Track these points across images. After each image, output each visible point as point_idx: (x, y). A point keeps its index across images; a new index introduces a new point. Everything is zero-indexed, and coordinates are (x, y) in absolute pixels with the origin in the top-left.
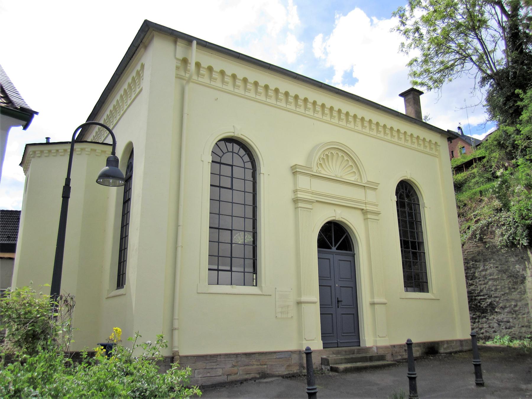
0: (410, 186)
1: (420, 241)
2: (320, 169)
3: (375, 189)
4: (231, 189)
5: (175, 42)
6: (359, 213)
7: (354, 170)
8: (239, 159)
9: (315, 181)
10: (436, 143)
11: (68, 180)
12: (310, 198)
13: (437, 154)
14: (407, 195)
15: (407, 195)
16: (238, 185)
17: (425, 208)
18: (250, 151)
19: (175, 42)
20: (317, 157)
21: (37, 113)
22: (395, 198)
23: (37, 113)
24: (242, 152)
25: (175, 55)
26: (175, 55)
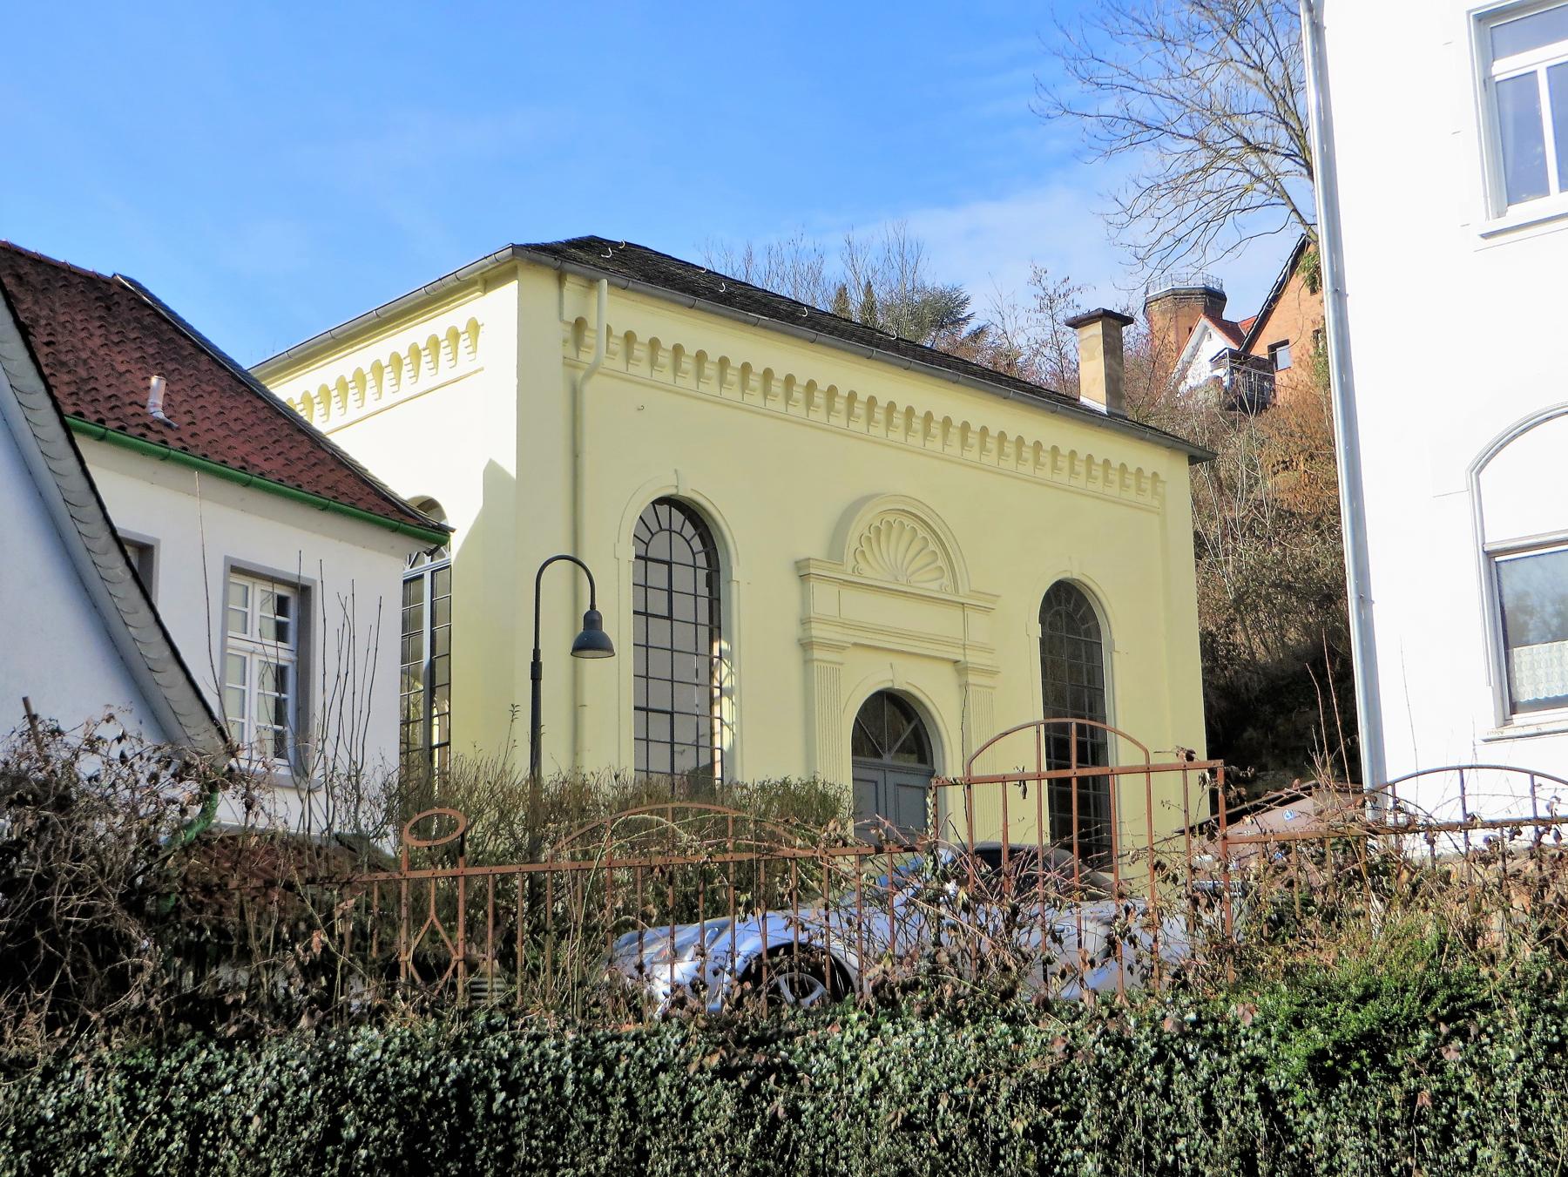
0: (1079, 592)
1: (1100, 740)
2: (862, 564)
3: (988, 610)
4: (670, 618)
5: (561, 279)
6: (948, 669)
7: (940, 563)
8: (686, 546)
9: (849, 594)
10: (1155, 474)
11: (536, 653)
12: (838, 637)
13: (1156, 503)
14: (1069, 617)
15: (1069, 617)
16: (683, 607)
17: (1115, 655)
18: (706, 527)
19: (561, 279)
20: (857, 535)
21: (453, 530)
22: (1037, 631)
23: (453, 530)
24: (689, 530)
25: (561, 314)
26: (561, 314)
